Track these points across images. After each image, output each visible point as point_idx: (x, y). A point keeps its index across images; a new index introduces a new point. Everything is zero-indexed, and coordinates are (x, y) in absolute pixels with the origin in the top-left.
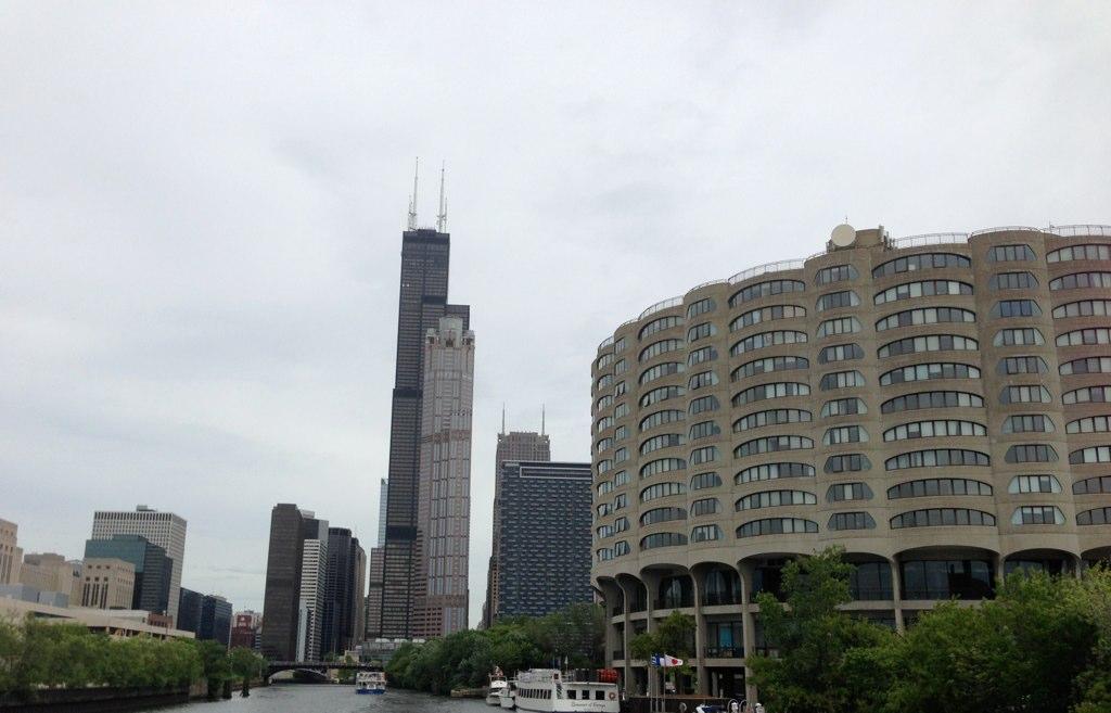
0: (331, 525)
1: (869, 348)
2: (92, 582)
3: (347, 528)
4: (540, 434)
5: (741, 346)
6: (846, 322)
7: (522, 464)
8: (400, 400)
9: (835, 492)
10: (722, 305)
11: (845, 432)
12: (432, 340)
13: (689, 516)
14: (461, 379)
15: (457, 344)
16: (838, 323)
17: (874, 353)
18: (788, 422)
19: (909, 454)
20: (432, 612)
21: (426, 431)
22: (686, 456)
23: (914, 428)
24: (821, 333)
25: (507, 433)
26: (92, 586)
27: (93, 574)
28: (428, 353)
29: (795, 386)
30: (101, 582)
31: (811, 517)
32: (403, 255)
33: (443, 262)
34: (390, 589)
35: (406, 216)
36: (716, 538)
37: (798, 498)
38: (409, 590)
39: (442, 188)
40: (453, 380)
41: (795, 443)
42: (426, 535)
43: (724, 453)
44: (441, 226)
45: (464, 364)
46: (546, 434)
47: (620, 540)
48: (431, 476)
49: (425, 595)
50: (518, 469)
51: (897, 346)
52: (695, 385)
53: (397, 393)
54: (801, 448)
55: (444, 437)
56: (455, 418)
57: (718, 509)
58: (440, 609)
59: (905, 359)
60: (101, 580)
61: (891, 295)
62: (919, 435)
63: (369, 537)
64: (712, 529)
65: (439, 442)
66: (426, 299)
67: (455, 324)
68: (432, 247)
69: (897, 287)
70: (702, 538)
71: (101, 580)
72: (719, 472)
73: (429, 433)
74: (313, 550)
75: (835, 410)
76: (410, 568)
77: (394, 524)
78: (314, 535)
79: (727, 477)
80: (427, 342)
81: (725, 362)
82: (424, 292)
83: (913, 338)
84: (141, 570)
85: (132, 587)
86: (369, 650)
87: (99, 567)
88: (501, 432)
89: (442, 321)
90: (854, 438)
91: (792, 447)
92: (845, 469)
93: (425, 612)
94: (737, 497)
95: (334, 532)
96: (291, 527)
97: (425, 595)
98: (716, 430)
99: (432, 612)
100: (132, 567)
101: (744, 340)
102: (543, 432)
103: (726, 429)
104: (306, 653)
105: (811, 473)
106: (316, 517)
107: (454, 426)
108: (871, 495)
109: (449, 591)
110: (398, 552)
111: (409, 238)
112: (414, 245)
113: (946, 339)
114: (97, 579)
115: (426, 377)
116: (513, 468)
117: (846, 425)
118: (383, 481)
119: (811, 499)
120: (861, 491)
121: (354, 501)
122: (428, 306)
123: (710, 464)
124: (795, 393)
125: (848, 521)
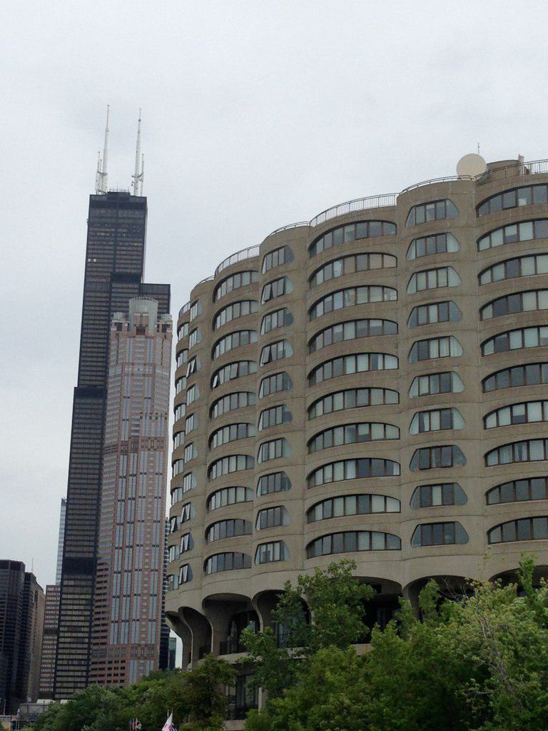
1: (468, 308)
5: (320, 307)
6: (442, 273)
8: (83, 401)
9: (423, 496)
10: (300, 253)
11: (436, 417)
12: (119, 326)
13: (254, 532)
14: (153, 375)
15: (151, 329)
16: (432, 275)
17: (476, 313)
18: (369, 405)
19: (513, 444)
20: (113, 665)
21: (109, 440)
22: (253, 451)
23: (519, 411)
24: (412, 290)
28: (113, 342)
29: (380, 358)
31: (392, 529)
33: (137, 232)
34: (66, 637)
35: (94, 176)
36: (281, 559)
37: (377, 505)
41: (377, 432)
43: (296, 444)
44: (136, 188)
45: (158, 357)
47: (183, 563)
49: (105, 644)
51: (501, 304)
52: (265, 359)
54: (385, 439)
55: (132, 446)
57: (286, 520)
59: (509, 321)
61: (497, 238)
62: (525, 419)
64: (277, 545)
65: (125, 453)
67: (149, 307)
68: (123, 213)
69: (504, 227)
70: (266, 560)
72: (289, 472)
75: (424, 390)
77: (73, 555)
79: (297, 476)
81: (303, 328)
83: (520, 293)
86: (28, 714)
90: (447, 424)
91: (374, 437)
92: (434, 465)
94: (308, 504)
97: (105, 644)
98: (287, 417)
99: (113, 665)
101: (322, 299)
103: (298, 413)
105: (396, 472)
108: (465, 500)
109: (135, 640)
110: (78, 590)
115: (111, 372)
117: (437, 407)
118: (63, 500)
119: (395, 507)
120: (451, 494)
123: (280, 461)
124: (380, 367)
125: (437, 534)
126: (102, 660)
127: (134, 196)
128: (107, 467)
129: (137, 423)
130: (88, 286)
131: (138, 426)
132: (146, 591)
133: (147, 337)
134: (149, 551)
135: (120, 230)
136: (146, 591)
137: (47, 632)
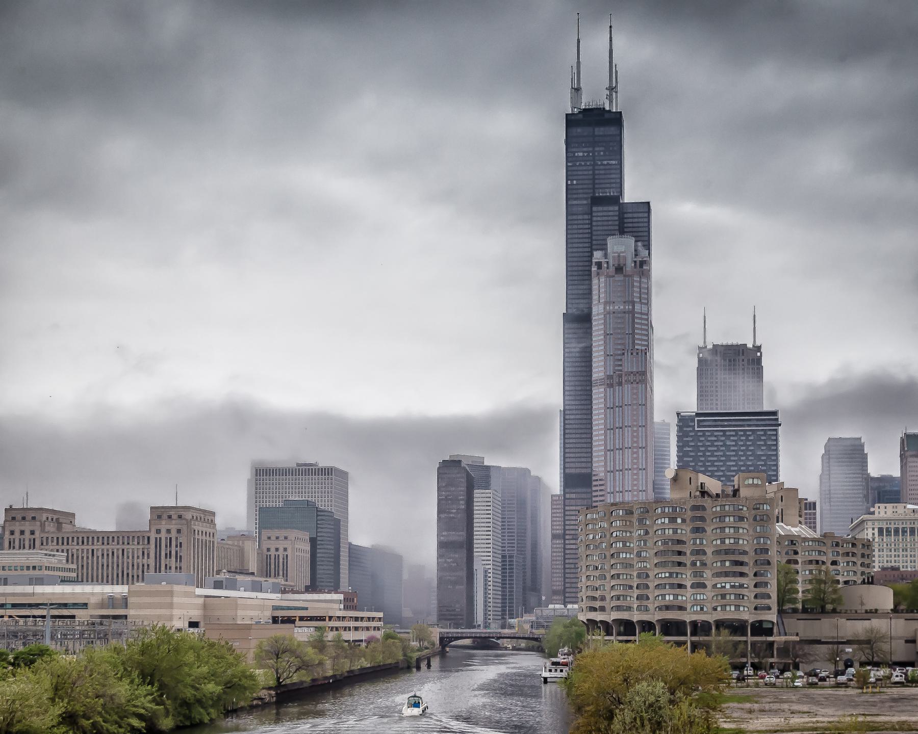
2: (273, 552)
12: (599, 265)
14: (632, 312)
15: (630, 265)
25: (710, 346)
26: (273, 557)
30: (281, 552)
44: (611, 102)
46: (758, 344)
60: (281, 550)
66: (597, 201)
68: (600, 131)
71: (281, 550)
77: (573, 471)
82: (594, 193)
88: (702, 345)
100: (306, 536)
104: (485, 606)
106: (486, 463)
111: (571, 121)
112: (356, 667)
113: (736, 529)
114: (277, 550)
122: (600, 208)
127: (609, 111)
128: (596, 420)
129: (619, 357)
130: (569, 236)
131: (621, 360)
132: (635, 445)
133: (625, 276)
134: (637, 474)
135: (597, 149)
137: (554, 537)
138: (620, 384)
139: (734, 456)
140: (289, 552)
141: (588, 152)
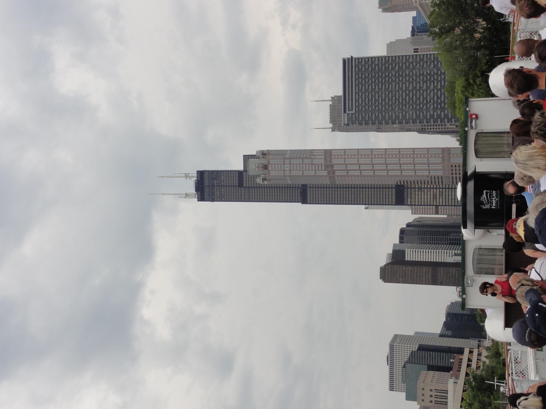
0: (397, 241)
2: (433, 393)
3: (399, 231)
4: (331, 103)
7: (345, 112)
8: (309, 199)
12: (264, 179)
15: (264, 162)
20: (454, 172)
21: (327, 182)
25: (331, 125)
26: (436, 399)
27: (427, 399)
30: (433, 393)
32: (213, 200)
33: (216, 175)
35: (188, 200)
38: (439, 188)
39: (168, 177)
40: (290, 164)
42: (400, 178)
44: (193, 177)
46: (330, 99)
48: (358, 176)
49: (442, 177)
50: (348, 114)
53: (304, 201)
55: (329, 167)
56: (316, 161)
58: (452, 166)
60: (431, 393)
63: (404, 216)
65: (334, 172)
66: (241, 184)
68: (206, 183)
71: (431, 393)
73: (328, 179)
74: (413, 254)
76: (424, 188)
77: (394, 200)
78: (403, 253)
80: (266, 182)
82: (236, 186)
84: (426, 367)
85: (437, 373)
87: (423, 395)
88: (330, 130)
89: (251, 173)
93: (454, 176)
95: (401, 239)
96: (398, 269)
99: (454, 172)
102: (329, 101)
106: (391, 252)
107: (322, 161)
110: (413, 196)
111: (202, 198)
112: (206, 194)
114: (431, 396)
116: (348, 118)
118: (366, 208)
121: (383, 227)
122: (245, 183)
126: (451, 179)
133: (269, 164)
135: (215, 185)
136: (412, 156)
138: (332, 166)
139: (434, 84)
140: (433, 388)
141: (217, 189)
